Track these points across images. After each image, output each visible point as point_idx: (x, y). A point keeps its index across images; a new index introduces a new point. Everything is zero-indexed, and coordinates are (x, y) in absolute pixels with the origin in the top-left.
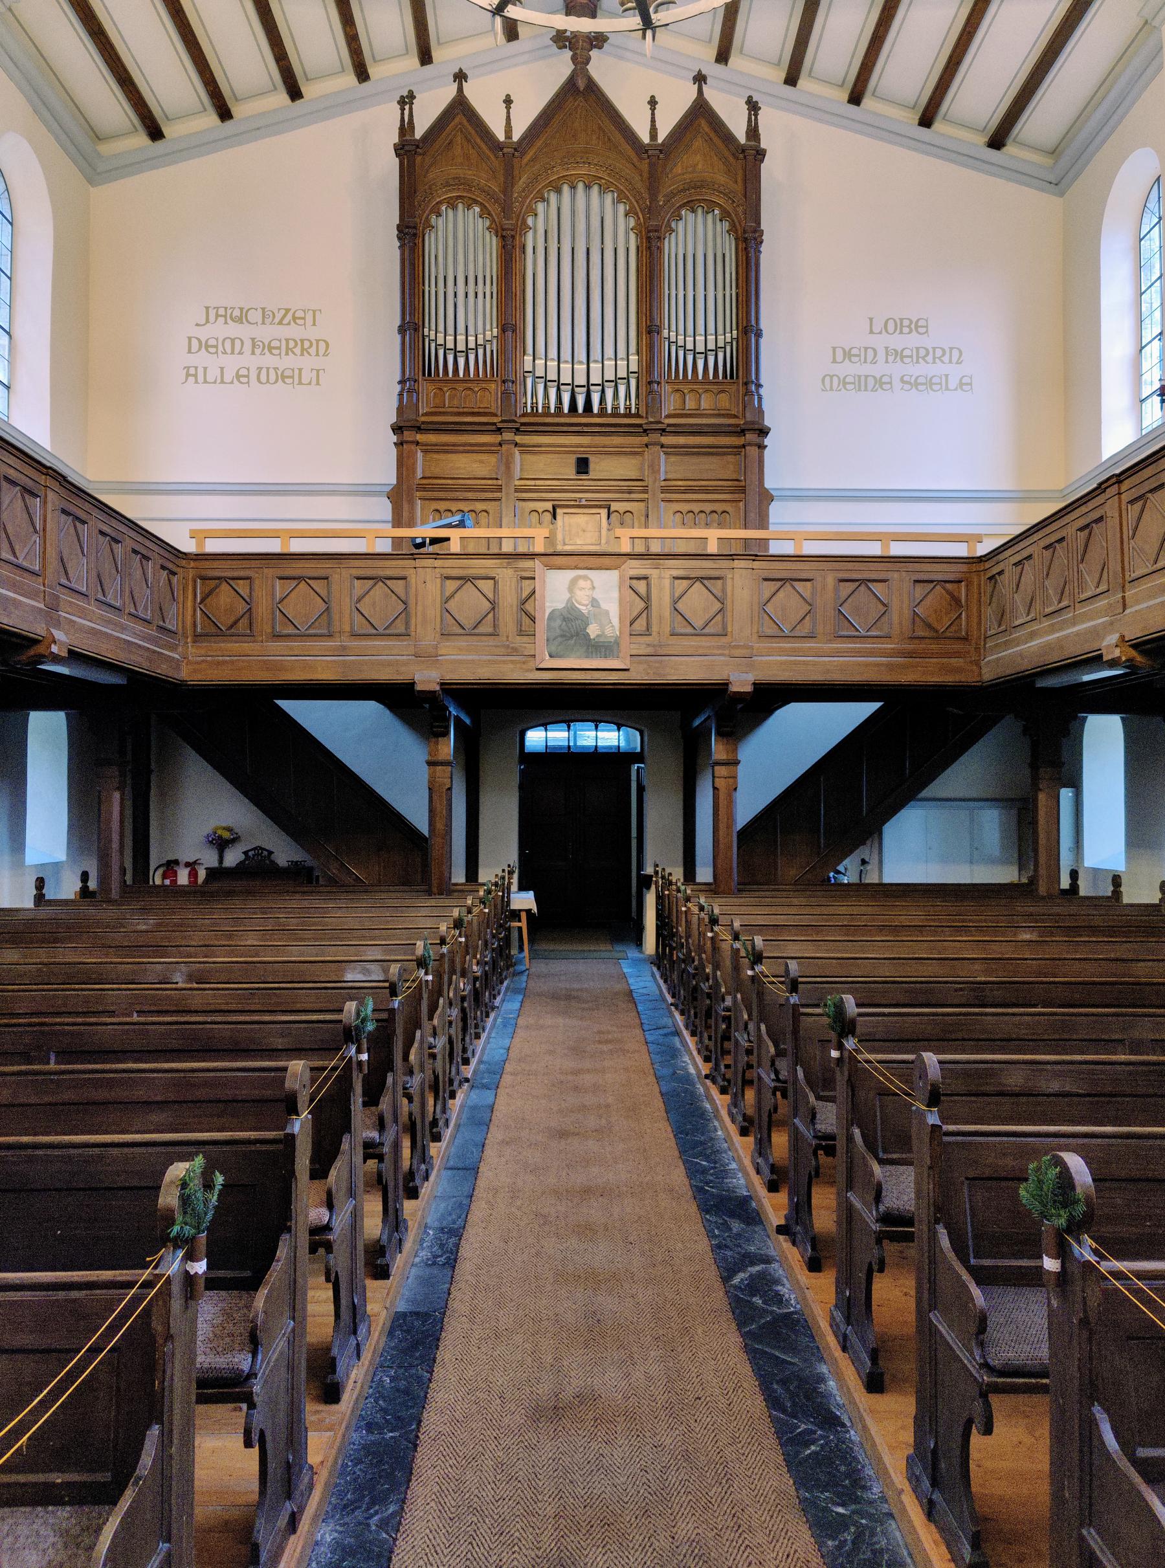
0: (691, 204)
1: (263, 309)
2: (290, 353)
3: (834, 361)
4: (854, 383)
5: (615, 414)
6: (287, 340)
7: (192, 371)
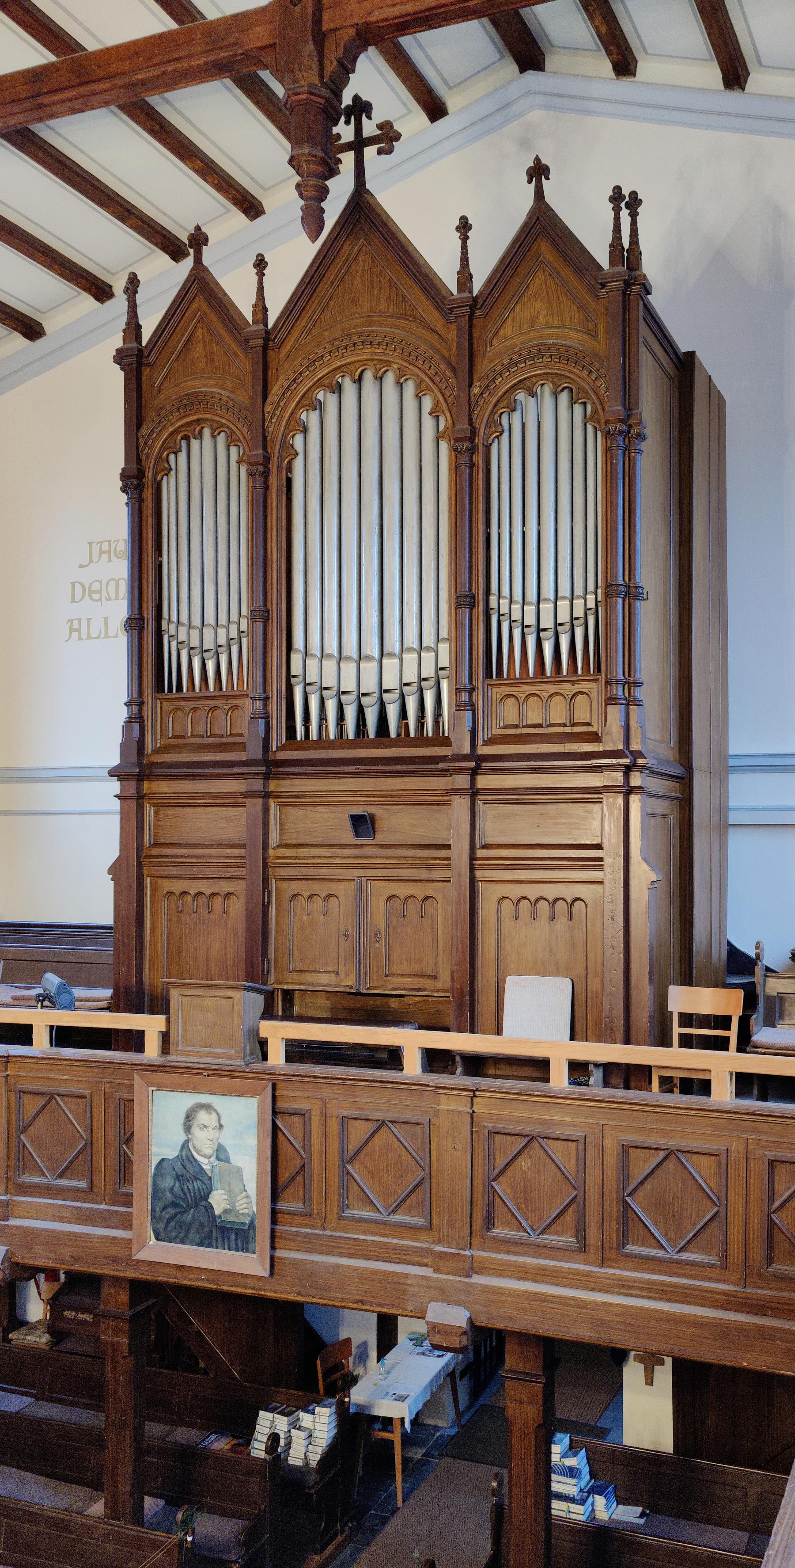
0: (528, 383)
5: (404, 739)
7: (76, 625)
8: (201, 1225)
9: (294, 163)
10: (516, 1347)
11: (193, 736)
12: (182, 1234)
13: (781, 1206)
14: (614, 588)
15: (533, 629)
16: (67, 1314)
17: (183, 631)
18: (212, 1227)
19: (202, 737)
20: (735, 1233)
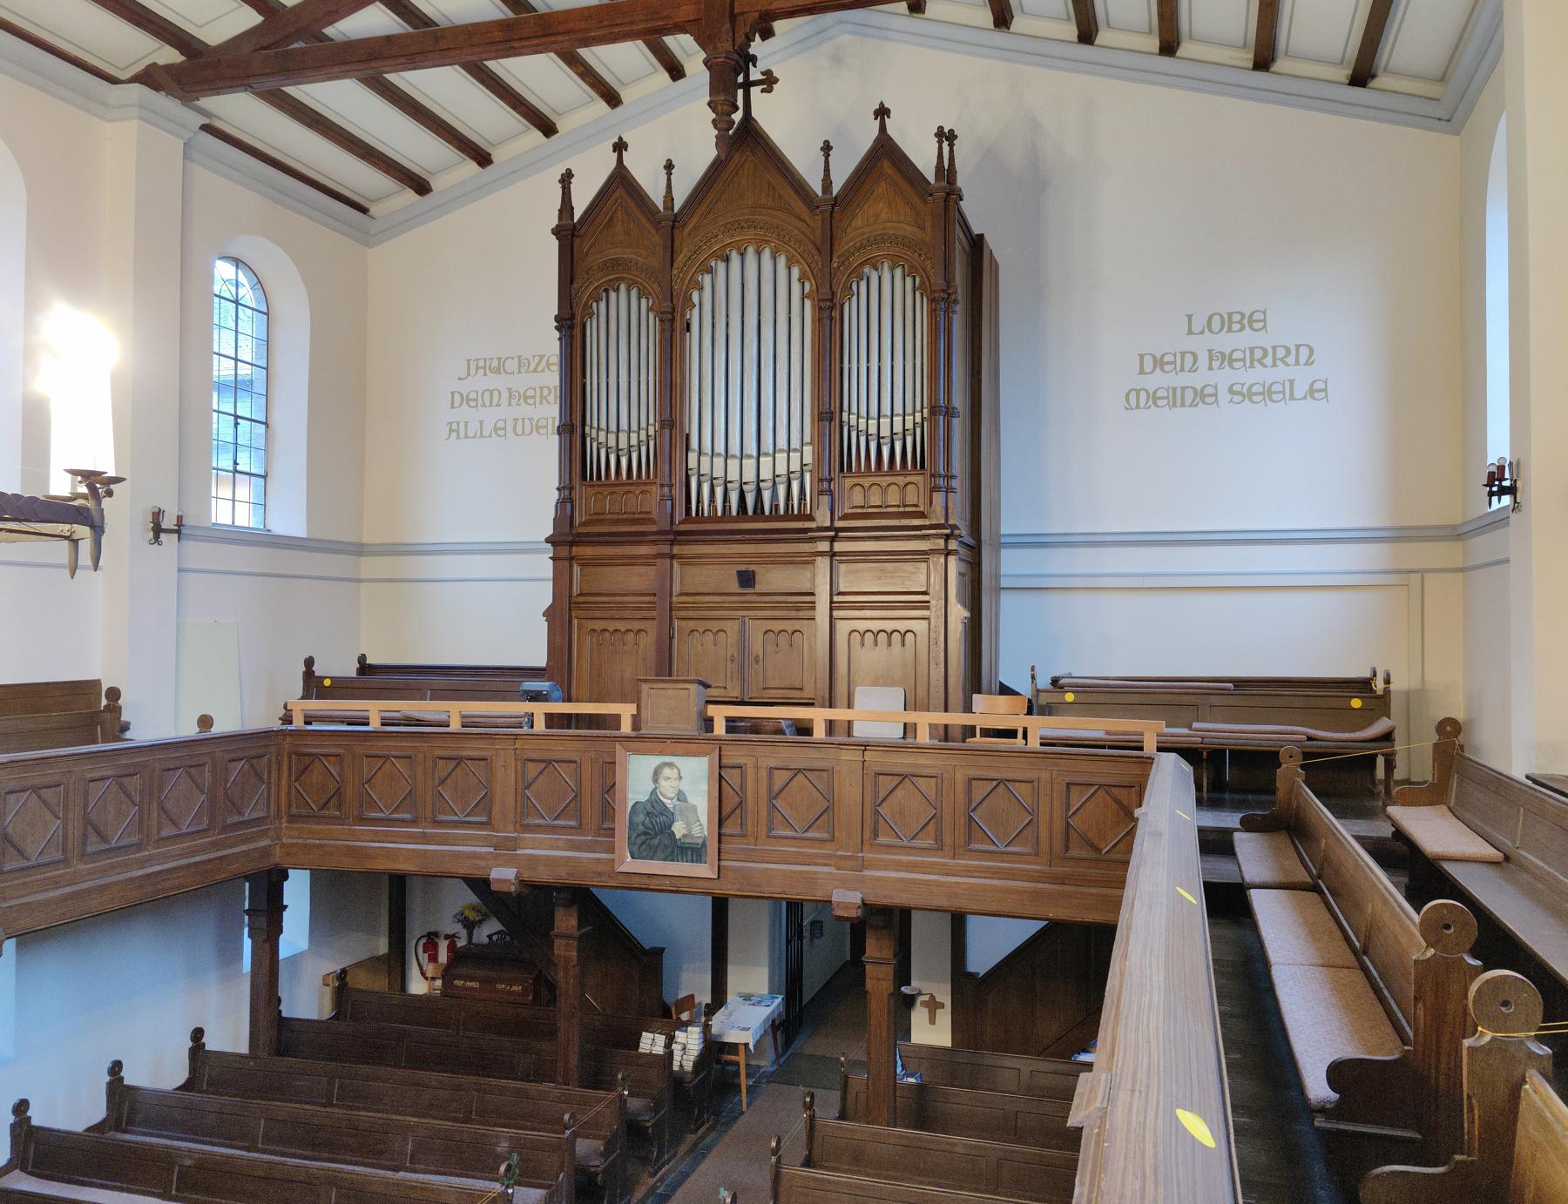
0: (874, 261)
1: (519, 357)
2: (544, 401)
3: (1142, 372)
4: (1167, 398)
6: (541, 388)
9: (712, 105)
10: (875, 942)
11: (610, 513)
12: (651, 854)
13: (1074, 813)
14: (937, 409)
15: (875, 437)
17: (602, 435)
18: (673, 848)
19: (618, 514)
20: (1044, 835)
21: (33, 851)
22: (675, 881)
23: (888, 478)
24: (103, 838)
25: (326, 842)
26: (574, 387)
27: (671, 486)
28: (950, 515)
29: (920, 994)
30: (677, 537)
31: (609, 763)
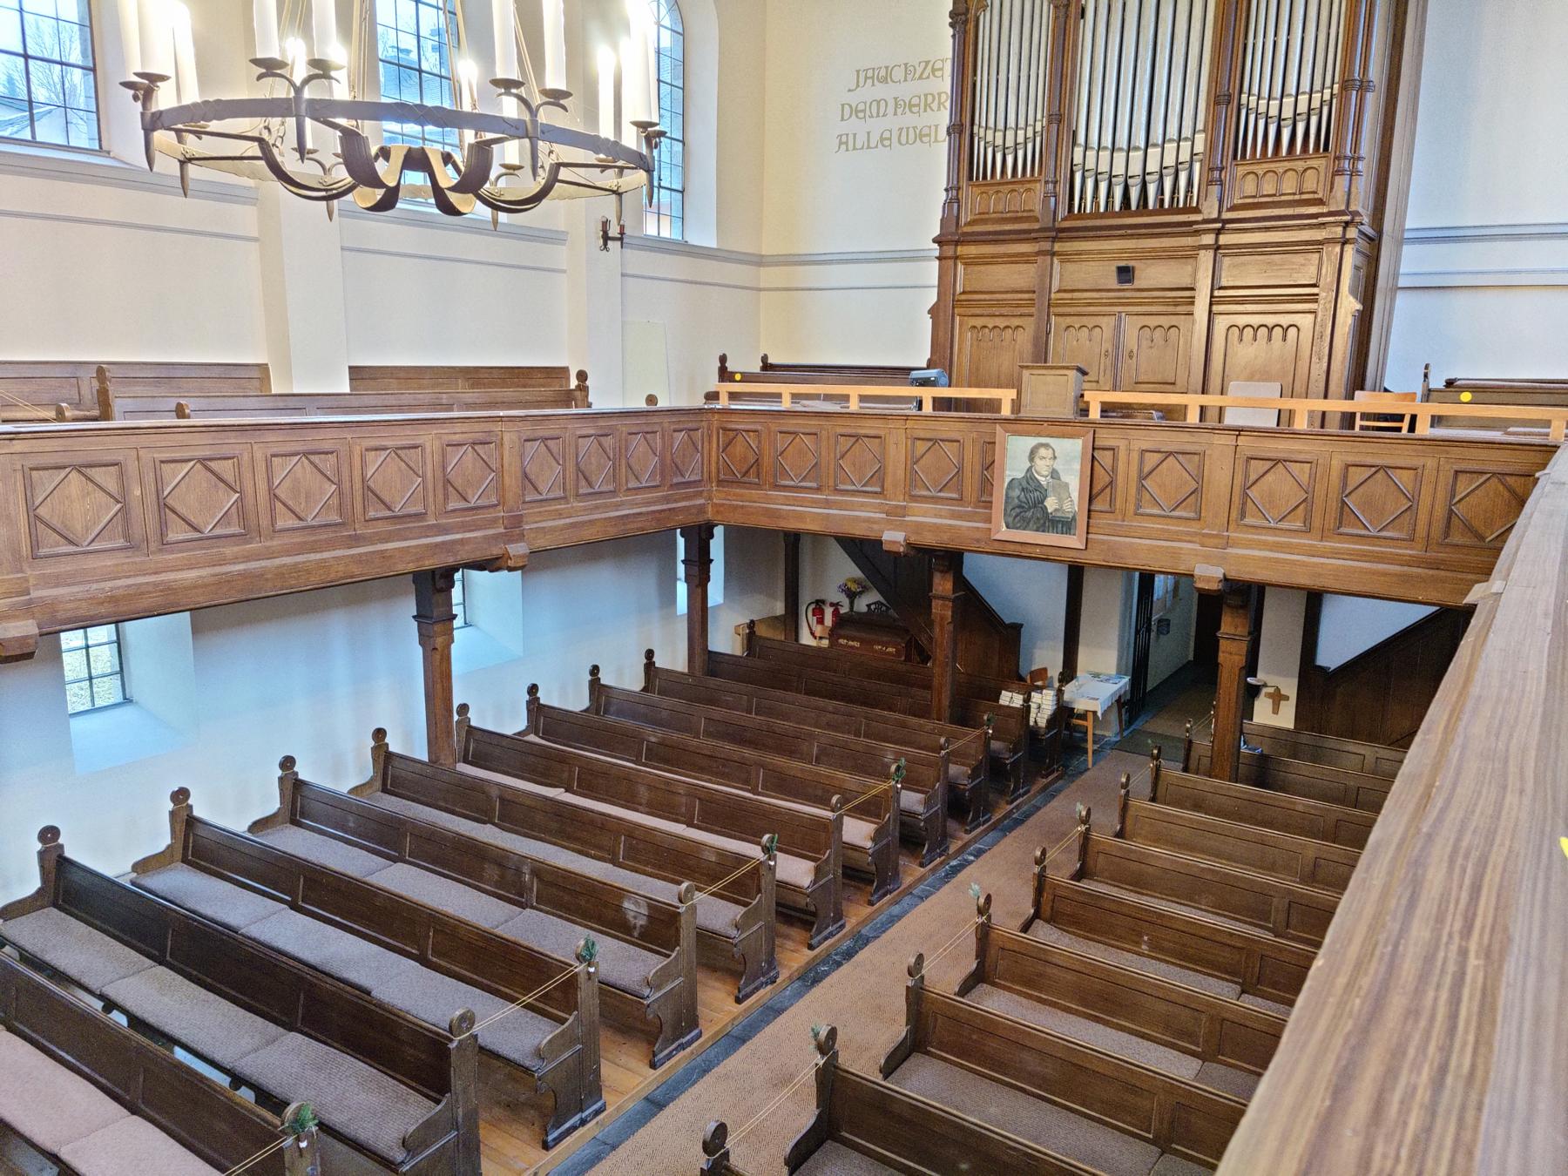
1: (906, 65)
2: (928, 109)
8: (1038, 519)
10: (1230, 619)
11: (994, 212)
14: (1350, 83)
15: (1276, 119)
16: (841, 641)
17: (990, 133)
21: (543, 488)
22: (1045, 550)
23: (1286, 164)
24: (590, 485)
25: (747, 504)
26: (965, 87)
27: (1055, 183)
28: (1352, 200)
29: (1265, 685)
30: (1059, 234)
31: (989, 443)
